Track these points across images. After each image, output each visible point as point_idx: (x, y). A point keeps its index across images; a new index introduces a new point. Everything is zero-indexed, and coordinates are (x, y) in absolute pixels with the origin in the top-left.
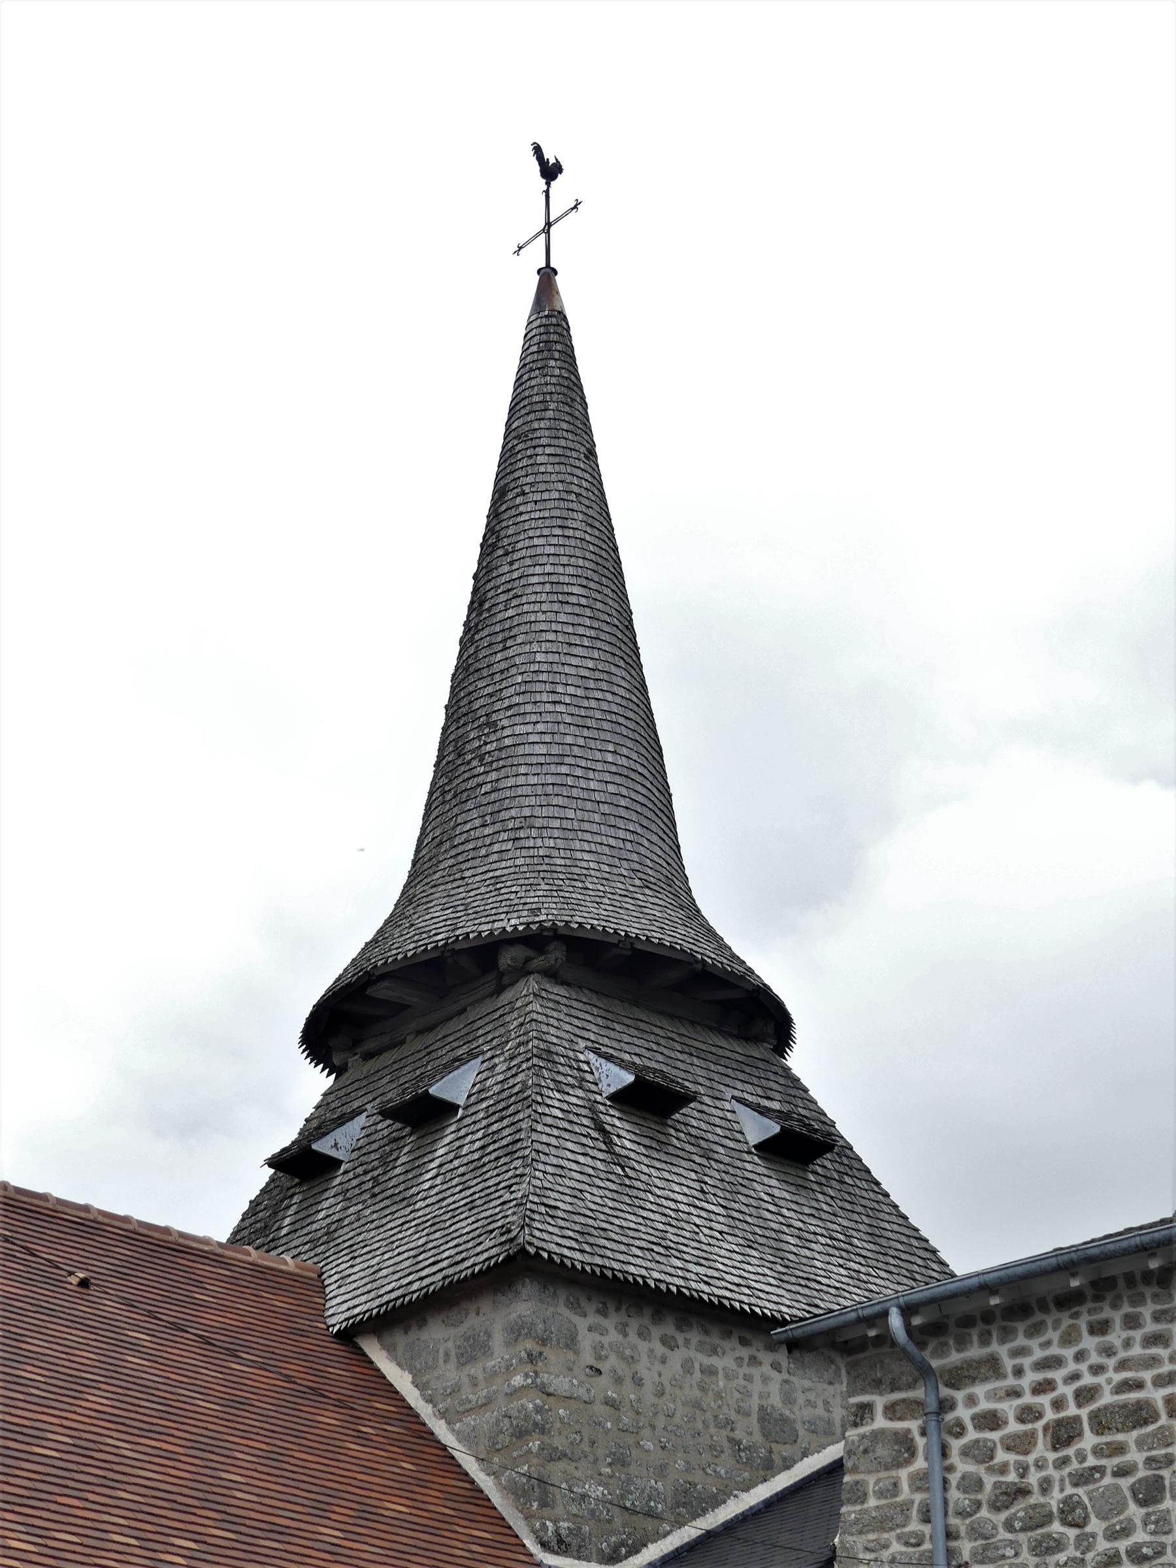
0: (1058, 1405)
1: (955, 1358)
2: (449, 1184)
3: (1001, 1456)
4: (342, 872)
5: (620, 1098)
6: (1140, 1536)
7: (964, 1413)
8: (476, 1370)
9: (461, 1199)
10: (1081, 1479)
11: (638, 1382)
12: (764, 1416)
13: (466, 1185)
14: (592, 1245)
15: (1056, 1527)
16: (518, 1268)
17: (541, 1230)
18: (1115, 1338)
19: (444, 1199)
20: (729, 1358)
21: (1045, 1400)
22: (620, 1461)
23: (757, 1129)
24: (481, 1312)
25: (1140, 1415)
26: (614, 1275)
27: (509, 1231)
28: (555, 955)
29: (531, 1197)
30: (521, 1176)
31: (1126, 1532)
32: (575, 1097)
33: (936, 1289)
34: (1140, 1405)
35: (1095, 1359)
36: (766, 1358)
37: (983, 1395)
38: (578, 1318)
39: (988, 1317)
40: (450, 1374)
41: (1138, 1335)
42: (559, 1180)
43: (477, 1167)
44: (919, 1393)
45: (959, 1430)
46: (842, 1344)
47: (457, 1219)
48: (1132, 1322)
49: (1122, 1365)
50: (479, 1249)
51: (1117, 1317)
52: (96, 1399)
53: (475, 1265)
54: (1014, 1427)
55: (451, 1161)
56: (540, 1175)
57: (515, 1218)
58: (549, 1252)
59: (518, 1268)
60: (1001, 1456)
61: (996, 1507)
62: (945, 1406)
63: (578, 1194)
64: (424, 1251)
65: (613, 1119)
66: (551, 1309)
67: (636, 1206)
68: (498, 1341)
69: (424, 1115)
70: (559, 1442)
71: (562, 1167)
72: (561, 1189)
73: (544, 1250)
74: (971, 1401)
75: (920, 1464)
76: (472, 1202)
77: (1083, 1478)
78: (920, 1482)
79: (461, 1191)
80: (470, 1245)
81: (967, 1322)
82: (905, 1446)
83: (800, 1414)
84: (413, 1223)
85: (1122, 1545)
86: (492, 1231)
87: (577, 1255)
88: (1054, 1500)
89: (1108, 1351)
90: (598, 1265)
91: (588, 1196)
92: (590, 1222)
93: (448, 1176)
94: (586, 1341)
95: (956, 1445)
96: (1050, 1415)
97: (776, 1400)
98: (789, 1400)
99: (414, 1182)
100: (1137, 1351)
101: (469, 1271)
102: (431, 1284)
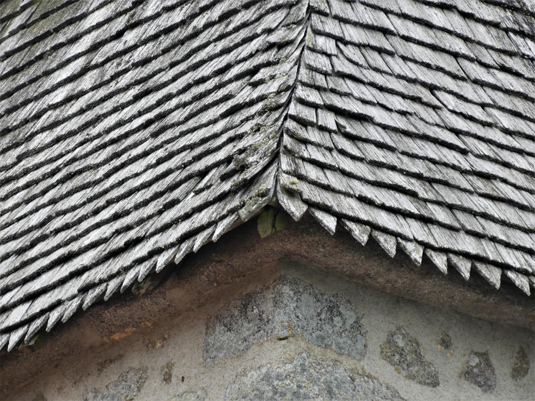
2: (113, 86)
13: (150, 83)
14: (451, 207)
17: (322, 166)
19: (98, 119)
24: (176, 372)
26: (505, 280)
27: (243, 168)
29: (300, 92)
30: (281, 46)
38: (416, 387)
42: (376, 59)
47: (124, 158)
50: (168, 216)
53: (158, 251)
55: (119, 35)
56: (330, 46)
57: (259, 137)
58: (340, 217)
63: (426, 95)
64: (44, 238)
66: (348, 363)
71: (386, 32)
72: (379, 79)
73: (328, 210)
76: (161, 116)
79: (137, 98)
80: (150, 209)
84: (22, 182)
86: (202, 174)
87: (413, 229)
90: (467, 255)
91: (451, 101)
92: (452, 157)
93: (111, 69)
99: (32, 91)
101: (142, 269)
102: (52, 307)
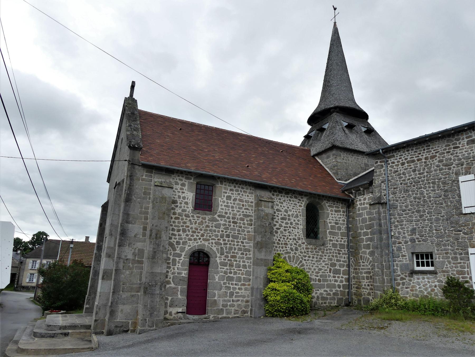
0: (402, 160)
1: (389, 155)
3: (395, 167)
4: (312, 103)
5: (346, 126)
6: (413, 176)
7: (390, 162)
8: (329, 159)
9: (326, 140)
10: (405, 169)
11: (349, 160)
12: (365, 164)
15: (402, 175)
16: (334, 147)
18: (410, 152)
20: (360, 157)
21: (400, 160)
22: (347, 170)
23: (364, 129)
25: (413, 161)
28: (338, 110)
31: (411, 176)
32: (340, 127)
33: (386, 147)
34: (413, 160)
35: (407, 155)
36: (365, 157)
37: (392, 160)
39: (393, 150)
40: (326, 160)
41: (413, 151)
43: (328, 136)
44: (384, 160)
45: (389, 164)
46: (374, 155)
48: (412, 150)
49: (411, 155)
51: (410, 149)
52: (283, 164)
54: (396, 163)
59: (334, 147)
60: (395, 167)
61: (394, 173)
62: (387, 161)
65: (345, 129)
67: (348, 139)
68: (331, 156)
69: (322, 130)
70: (339, 168)
74: (391, 160)
75: (384, 168)
77: (405, 169)
78: (384, 170)
81: (390, 151)
82: (382, 166)
83: (369, 163)
85: (411, 177)
88: (402, 172)
89: (409, 154)
94: (342, 155)
95: (389, 166)
96: (401, 162)
97: (366, 162)
98: (368, 162)
100: (413, 153)
